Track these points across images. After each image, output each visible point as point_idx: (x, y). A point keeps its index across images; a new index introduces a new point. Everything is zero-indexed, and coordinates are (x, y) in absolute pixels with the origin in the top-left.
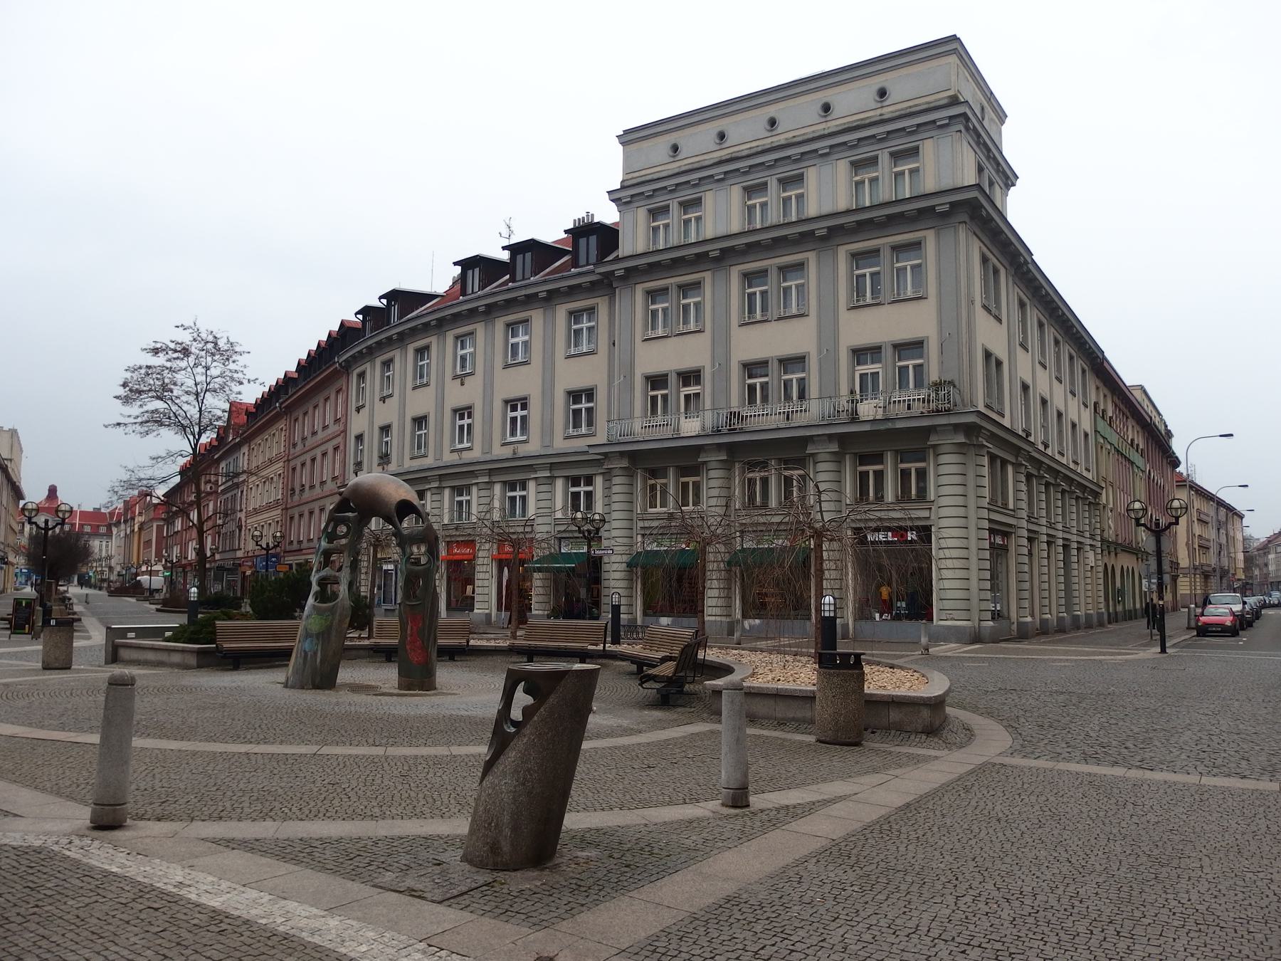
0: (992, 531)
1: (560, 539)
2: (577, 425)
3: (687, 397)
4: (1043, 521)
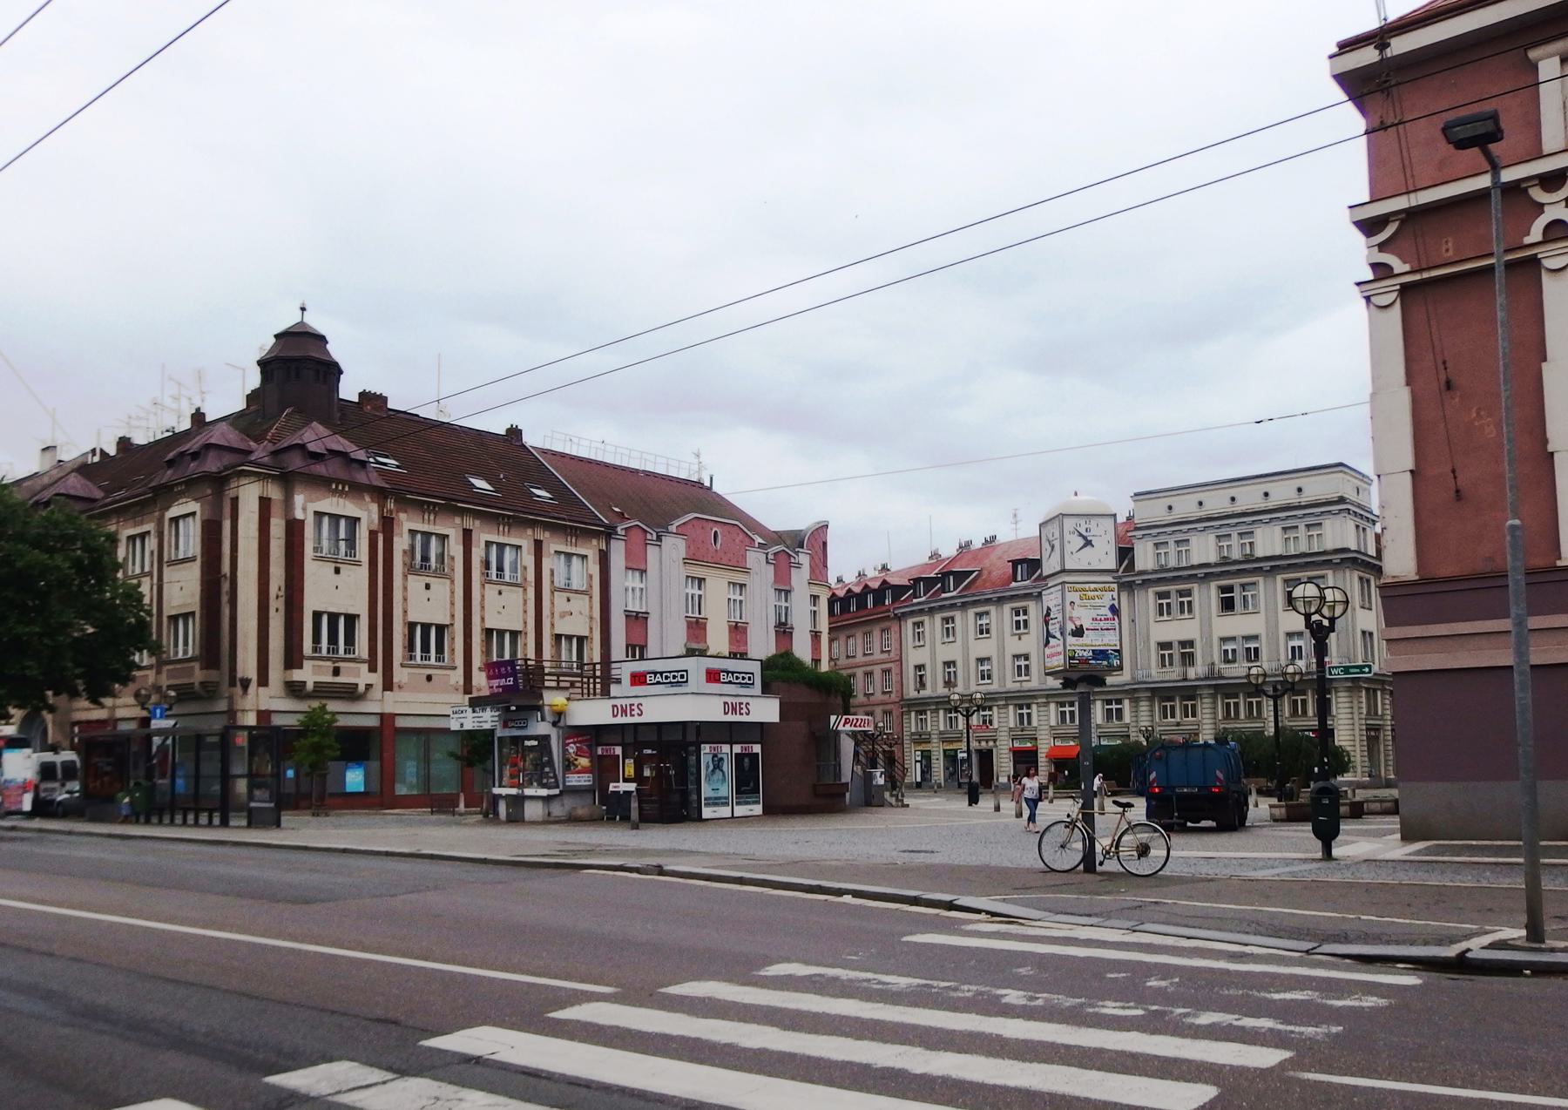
0: (1367, 730)
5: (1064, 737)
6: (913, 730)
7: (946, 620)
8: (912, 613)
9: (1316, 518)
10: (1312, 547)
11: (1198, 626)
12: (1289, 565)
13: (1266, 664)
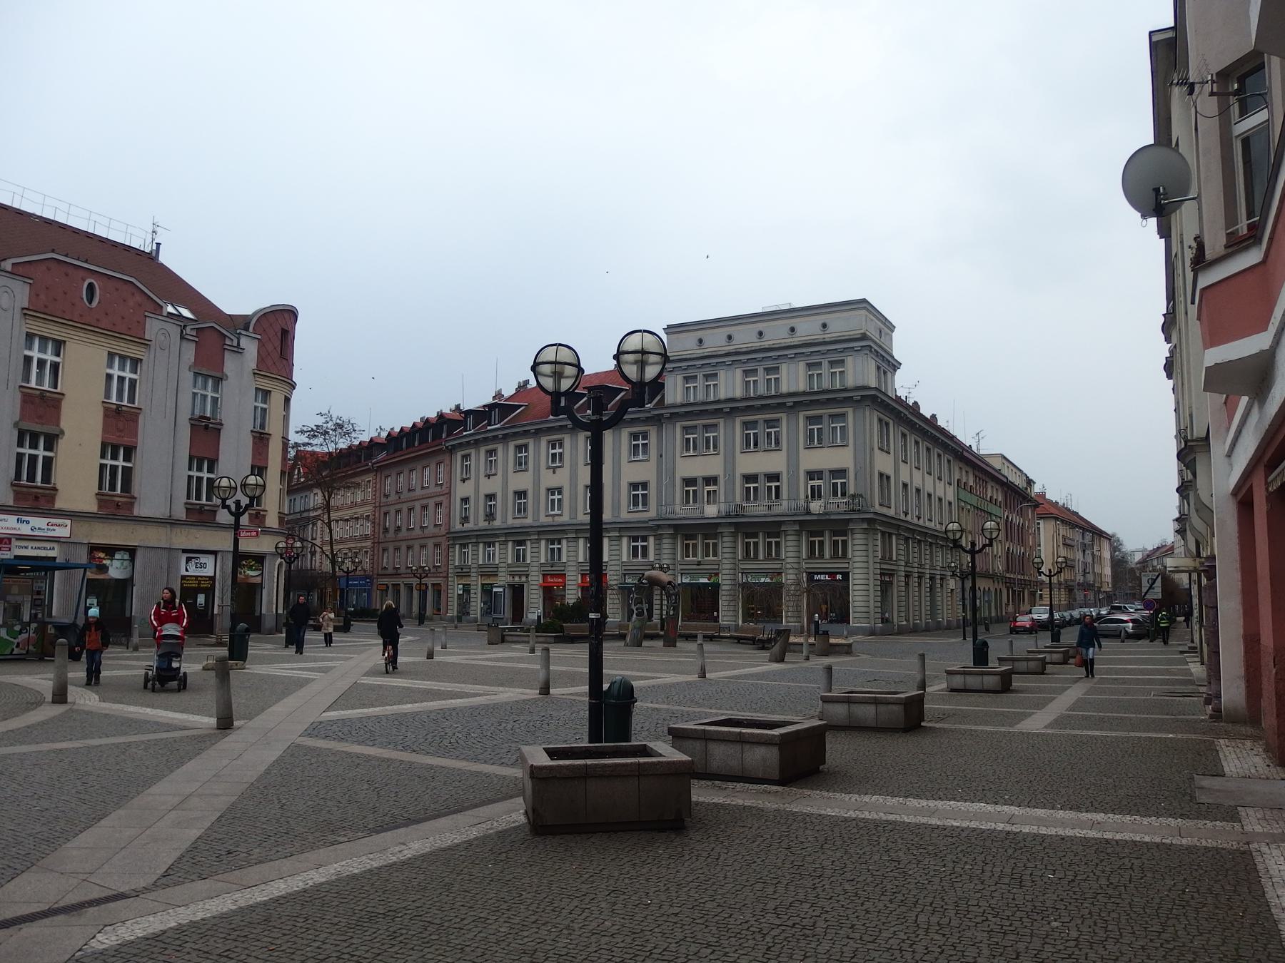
0: (881, 574)
1: (625, 575)
2: (636, 504)
3: (709, 492)
4: (916, 565)
7: (519, 448)
10: (812, 386)
11: (852, 456)
12: (828, 399)
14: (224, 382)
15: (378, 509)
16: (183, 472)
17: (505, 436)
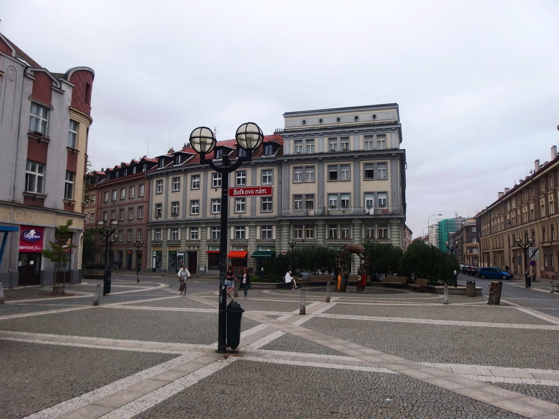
5: (214, 246)
6: (153, 240)
7: (175, 179)
8: (157, 175)
9: (311, 137)
13: (352, 210)
14: (51, 112)
15: (99, 210)
16: (23, 171)
17: (167, 173)
